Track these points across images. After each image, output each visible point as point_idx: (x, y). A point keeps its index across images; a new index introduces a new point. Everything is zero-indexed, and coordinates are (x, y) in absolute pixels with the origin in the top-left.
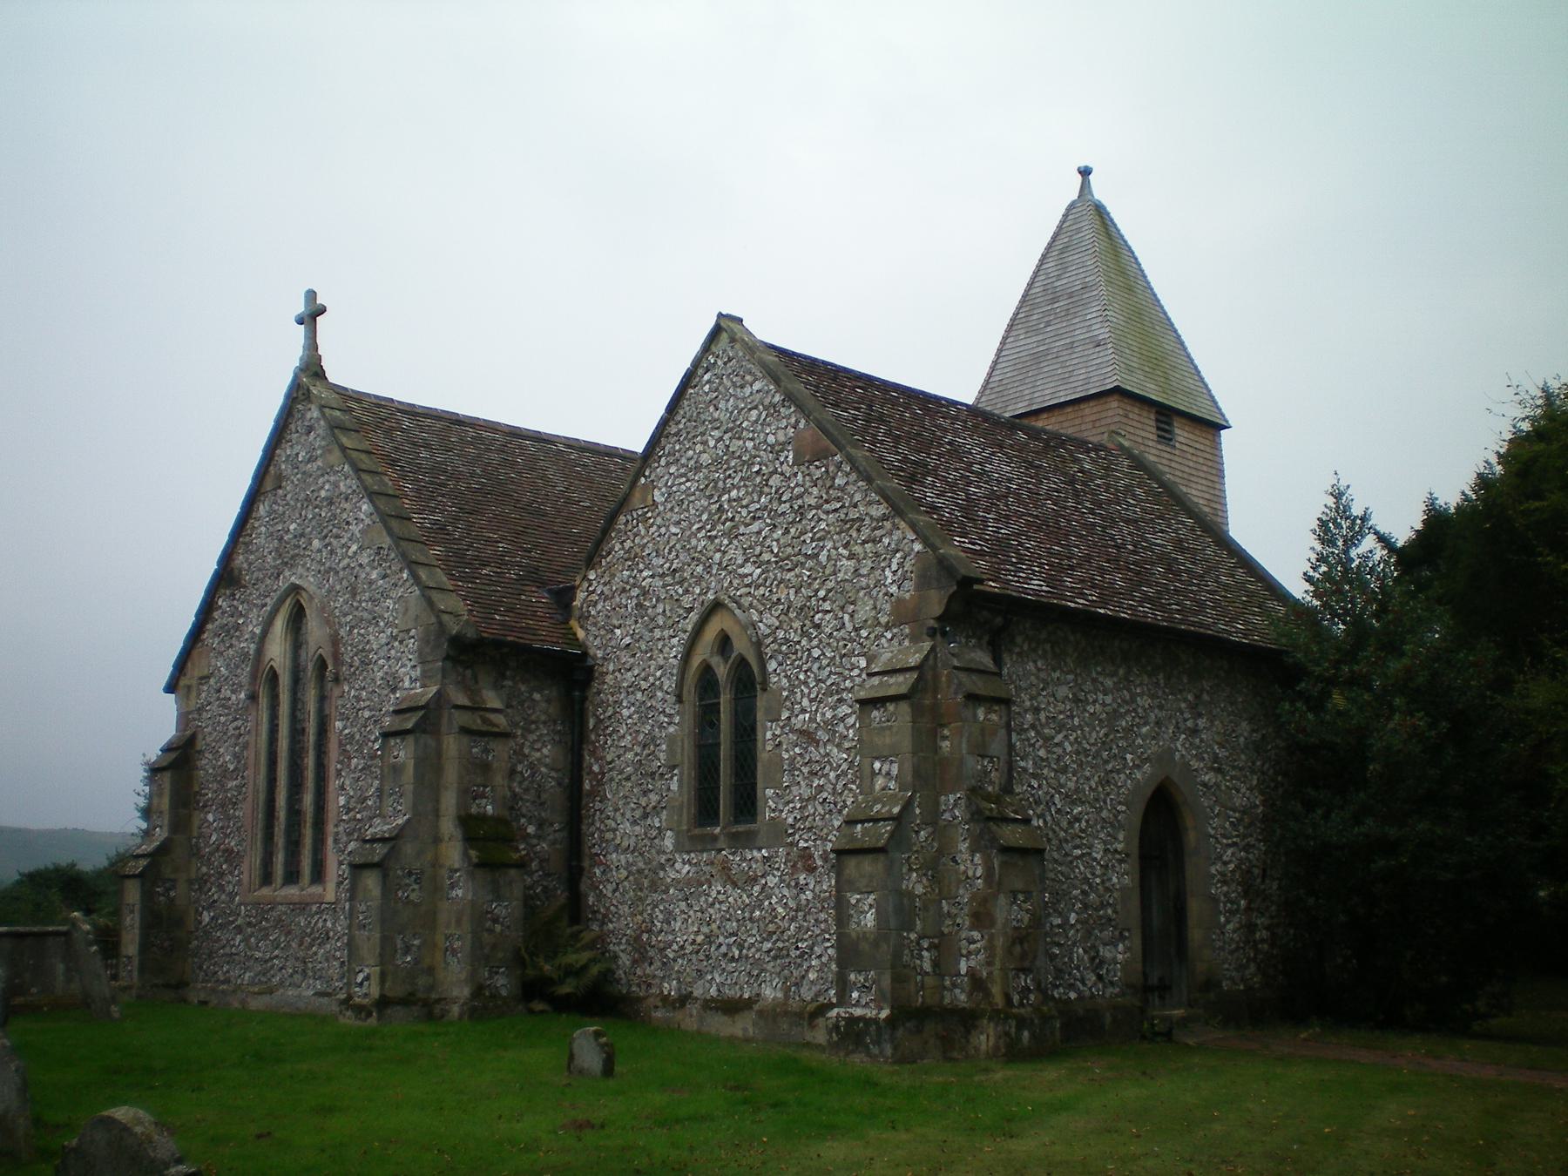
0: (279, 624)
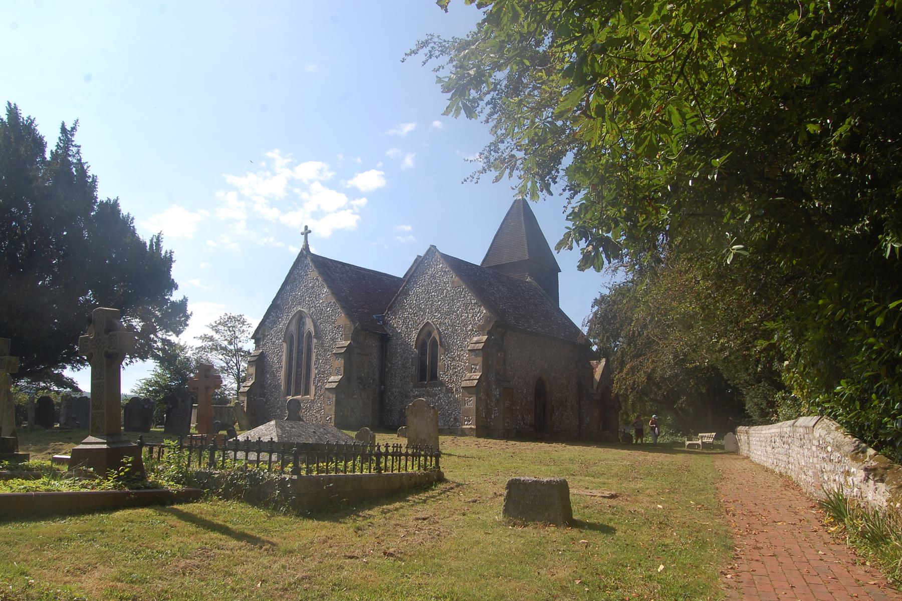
0: (294, 321)
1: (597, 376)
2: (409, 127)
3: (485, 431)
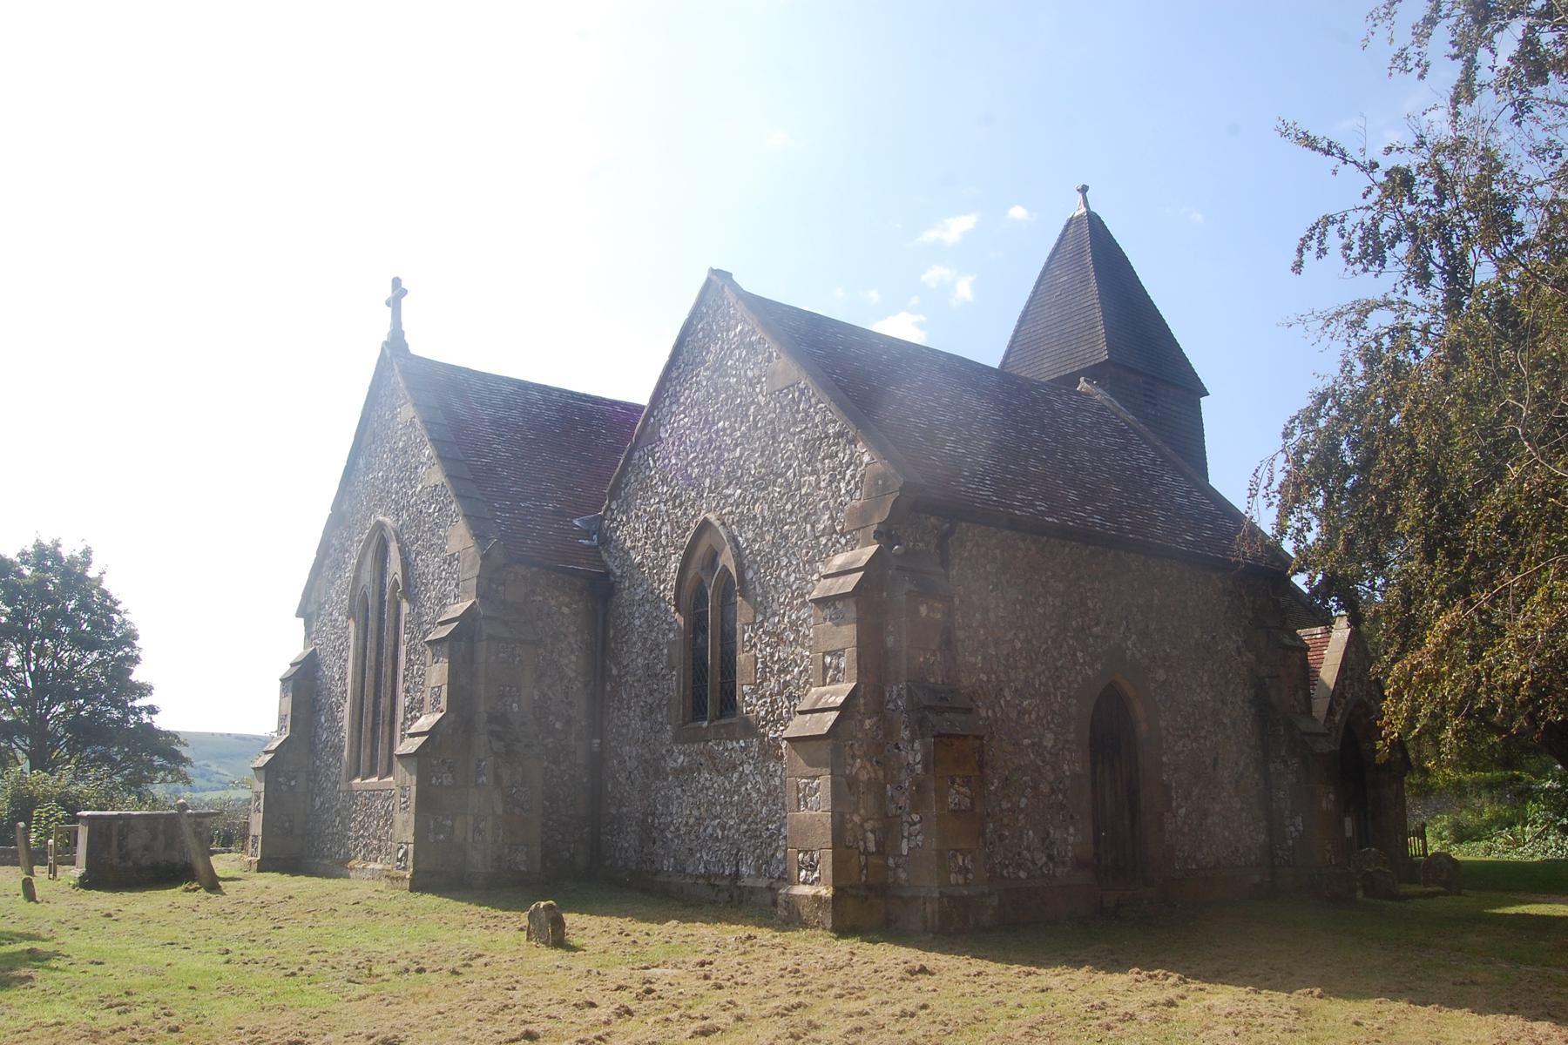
1: (1328, 672)
2: (966, 222)
3: (867, 908)
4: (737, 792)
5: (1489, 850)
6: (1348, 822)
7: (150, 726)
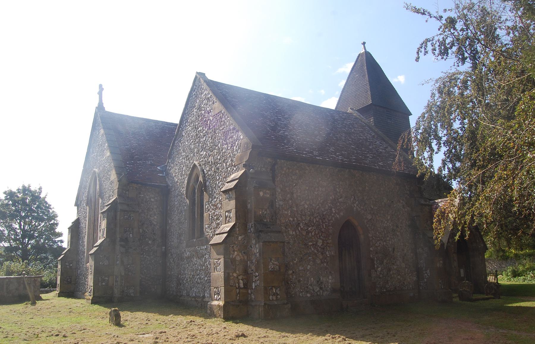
3: (238, 309)
4: (204, 265)
5: (524, 280)
6: (462, 271)
7: (61, 247)
